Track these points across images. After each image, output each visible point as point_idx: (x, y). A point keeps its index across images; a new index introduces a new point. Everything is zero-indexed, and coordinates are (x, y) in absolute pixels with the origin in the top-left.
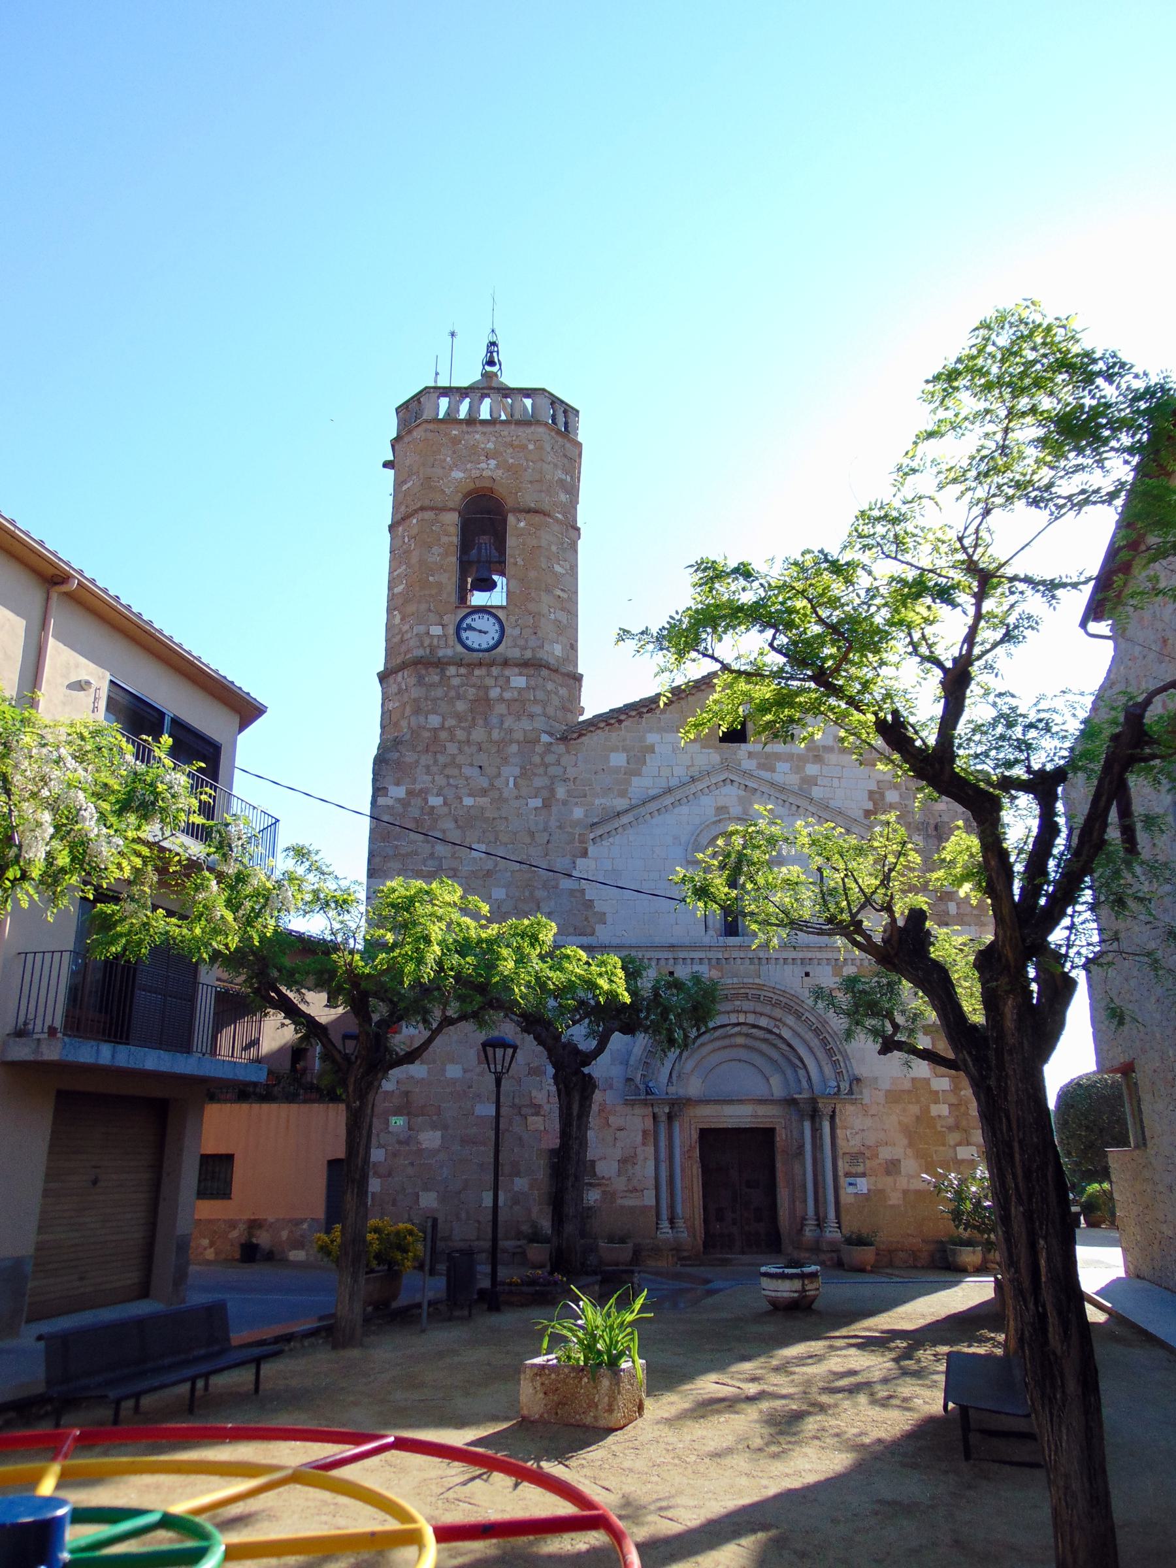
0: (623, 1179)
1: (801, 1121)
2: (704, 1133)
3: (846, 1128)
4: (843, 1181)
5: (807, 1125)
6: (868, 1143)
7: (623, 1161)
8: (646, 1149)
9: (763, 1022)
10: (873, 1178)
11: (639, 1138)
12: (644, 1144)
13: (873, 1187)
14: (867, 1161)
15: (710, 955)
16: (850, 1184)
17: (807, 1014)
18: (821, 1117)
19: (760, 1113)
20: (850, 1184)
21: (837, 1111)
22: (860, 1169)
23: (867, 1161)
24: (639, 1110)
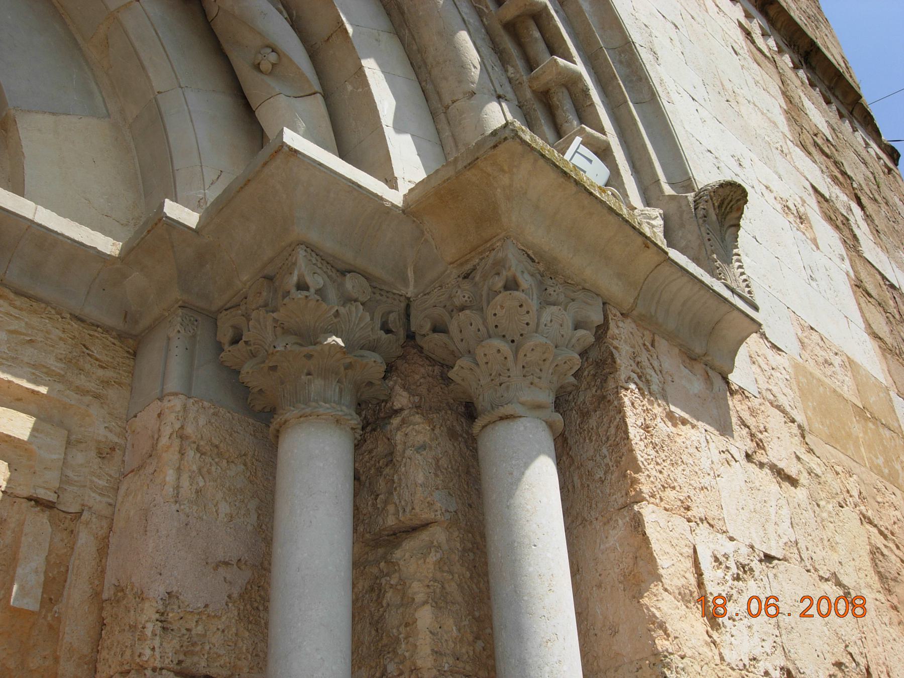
1: (261, 415)
5: (317, 468)
18: (466, 419)
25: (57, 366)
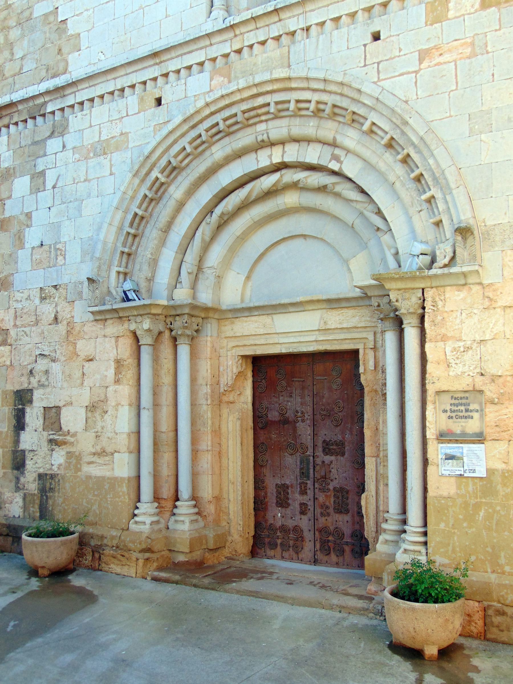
0: (91, 435)
2: (262, 366)
3: (444, 338)
4: (437, 451)
6: (492, 369)
7: (91, 408)
8: (120, 387)
9: (312, 155)
10: (502, 447)
11: (111, 373)
12: (117, 381)
13: (499, 466)
14: (489, 409)
15: (215, 51)
16: (450, 457)
17: (373, 117)
19: (332, 325)
20: (450, 457)
21: (428, 305)
22: (472, 426)
23: (489, 409)
24: (113, 328)
25: (368, 319)
